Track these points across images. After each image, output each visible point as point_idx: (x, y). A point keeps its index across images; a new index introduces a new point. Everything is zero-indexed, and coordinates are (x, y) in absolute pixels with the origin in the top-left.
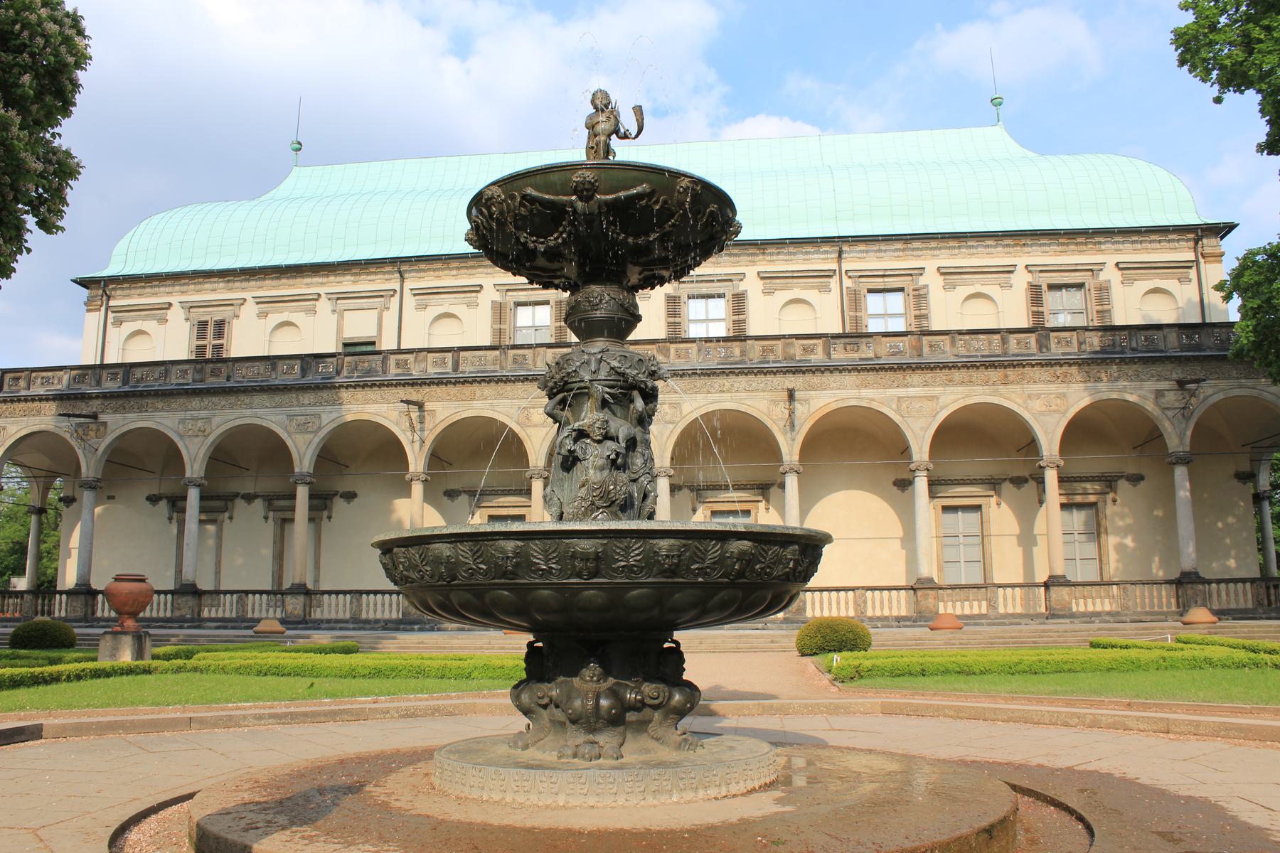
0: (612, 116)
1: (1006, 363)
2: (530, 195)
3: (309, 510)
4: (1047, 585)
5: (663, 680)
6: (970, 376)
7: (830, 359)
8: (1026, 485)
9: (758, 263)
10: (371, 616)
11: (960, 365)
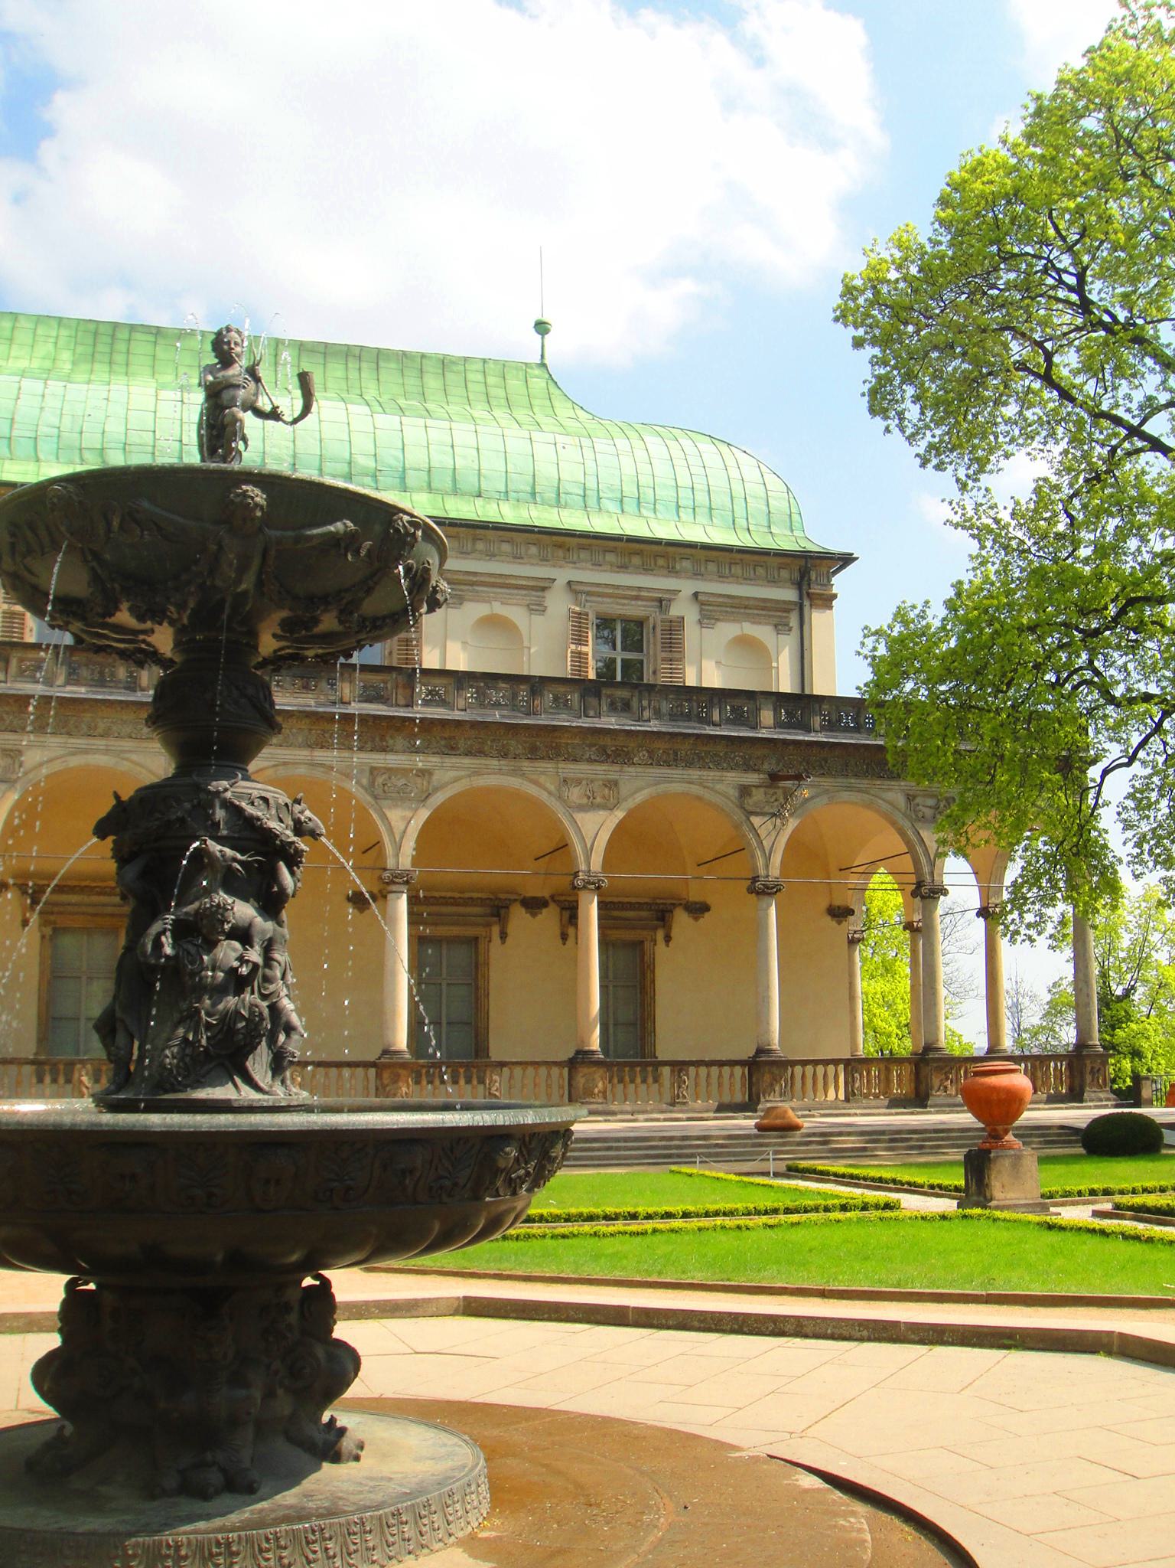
8: (544, 911)
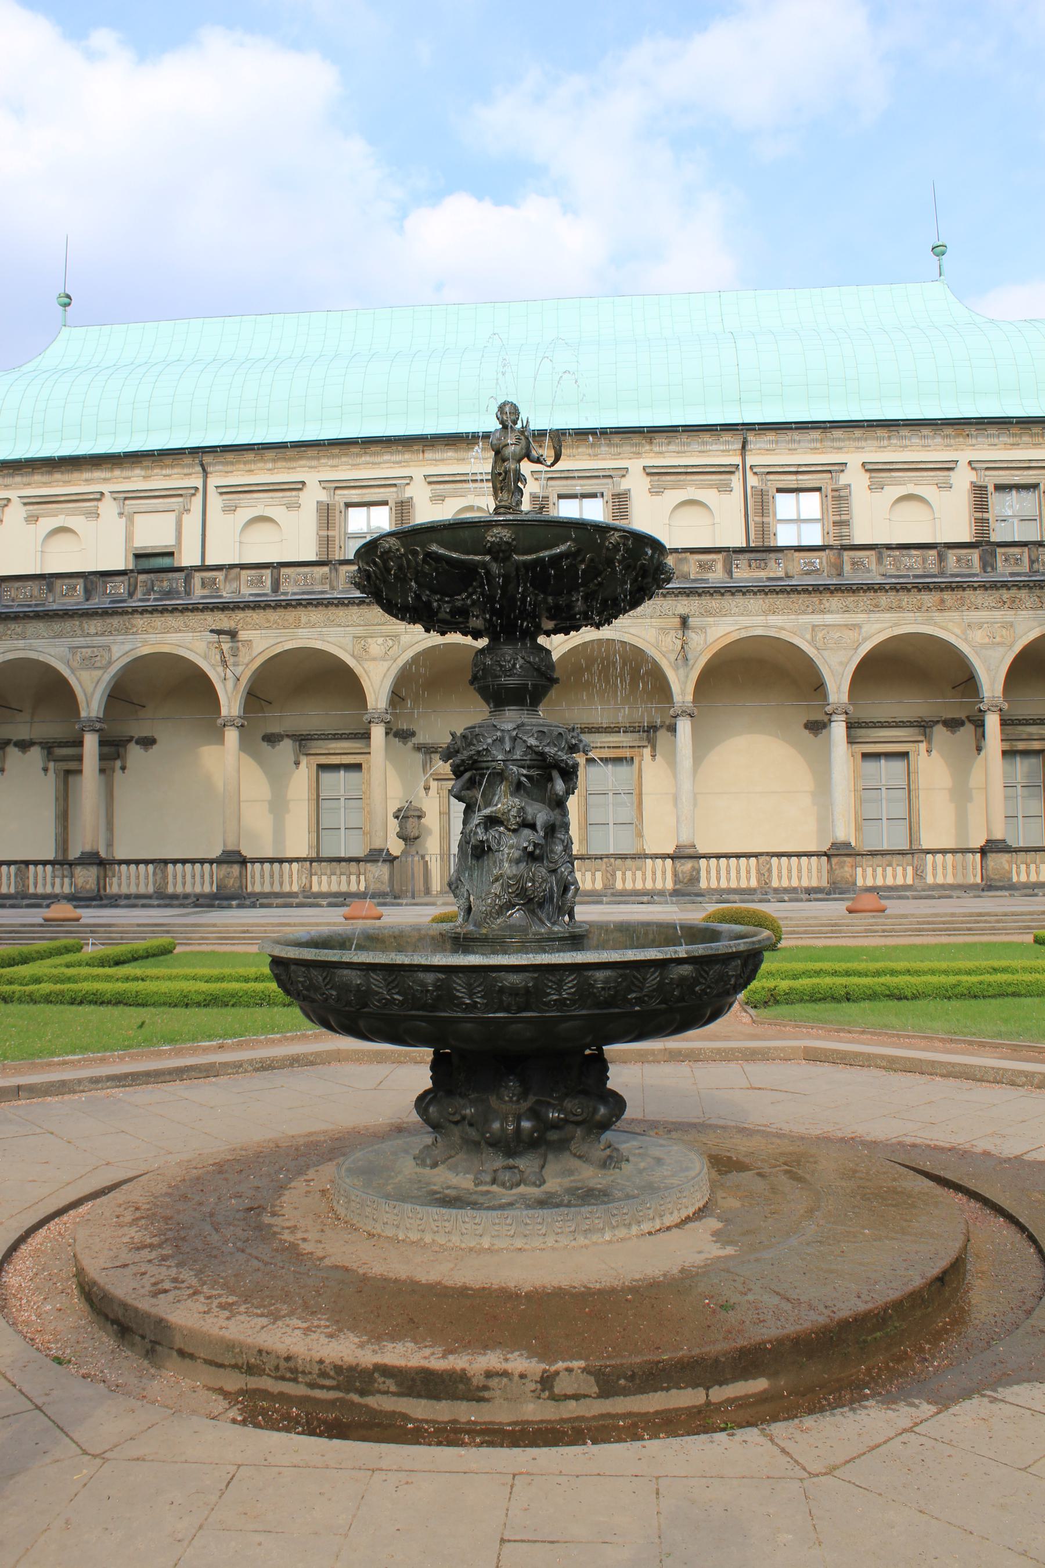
0: (522, 437)
1: (943, 585)
2: (436, 553)
3: (100, 759)
4: (983, 852)
5: (585, 1093)
6: (900, 600)
7: (731, 577)
8: (962, 729)
10: (179, 890)
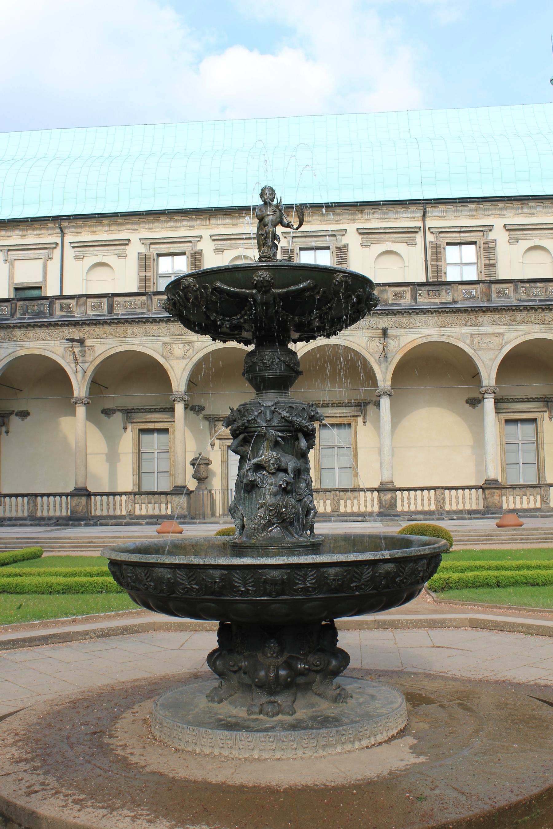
2: (220, 288)
6: (530, 317)
7: (416, 303)
9: (357, 221)
10: (45, 514)
11: (521, 308)
